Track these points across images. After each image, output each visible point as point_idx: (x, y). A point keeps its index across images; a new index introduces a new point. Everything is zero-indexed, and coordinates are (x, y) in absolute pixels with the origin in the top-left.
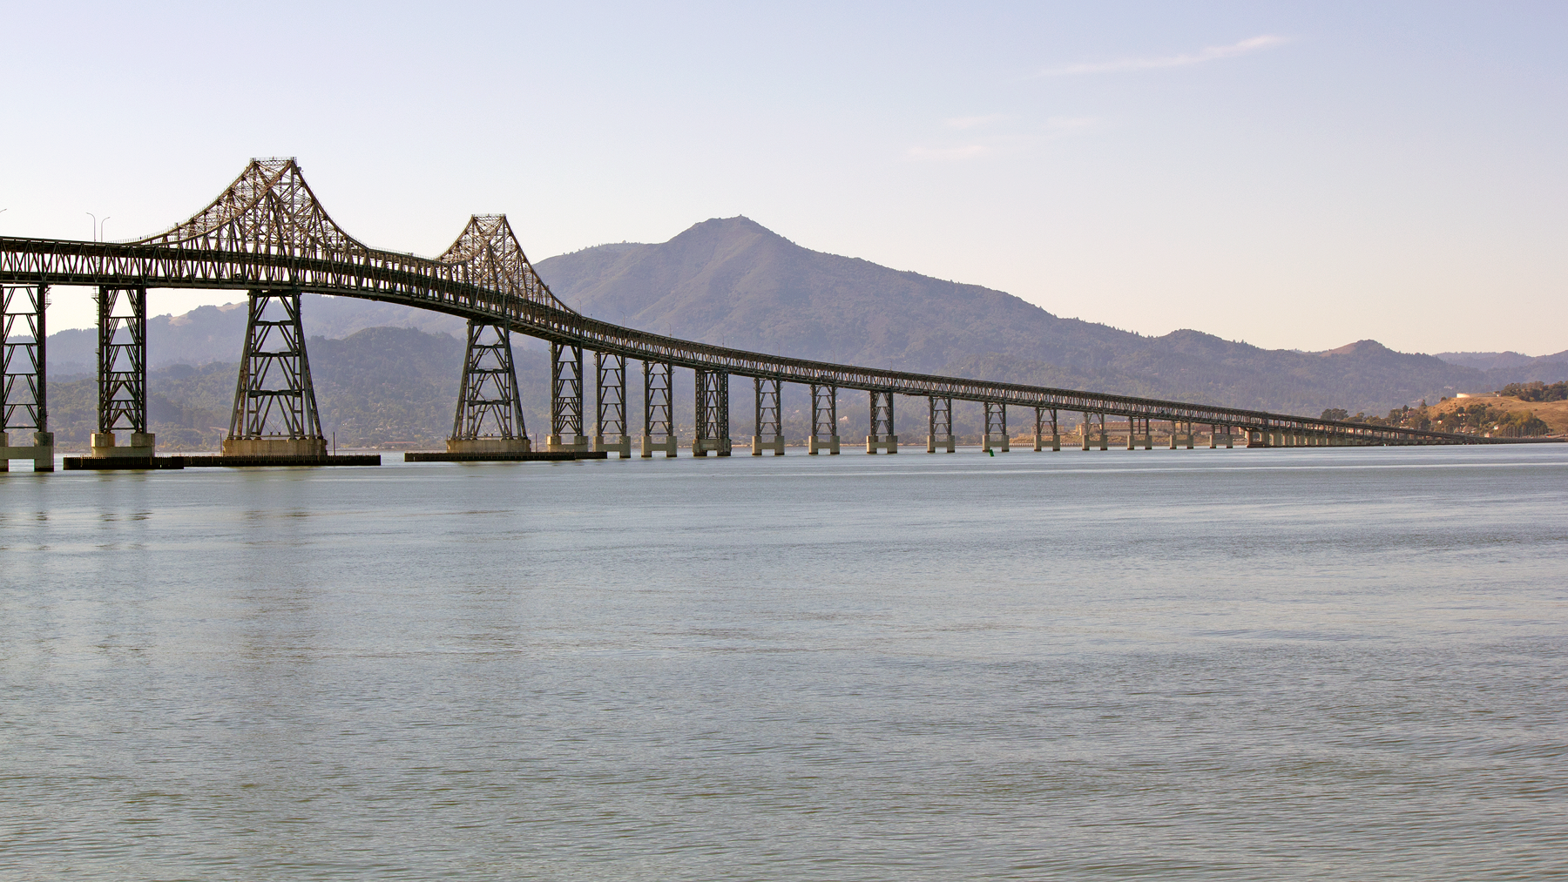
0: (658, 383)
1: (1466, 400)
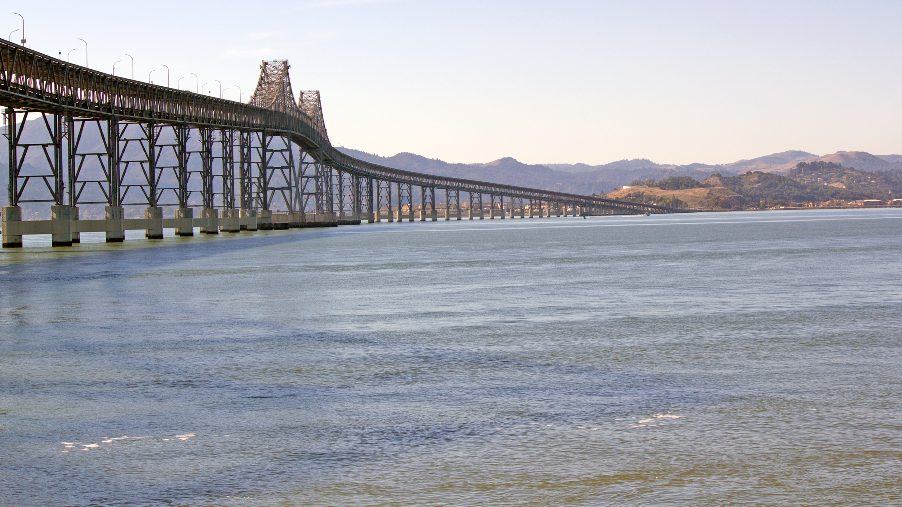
0: (405, 193)
1: (629, 190)
